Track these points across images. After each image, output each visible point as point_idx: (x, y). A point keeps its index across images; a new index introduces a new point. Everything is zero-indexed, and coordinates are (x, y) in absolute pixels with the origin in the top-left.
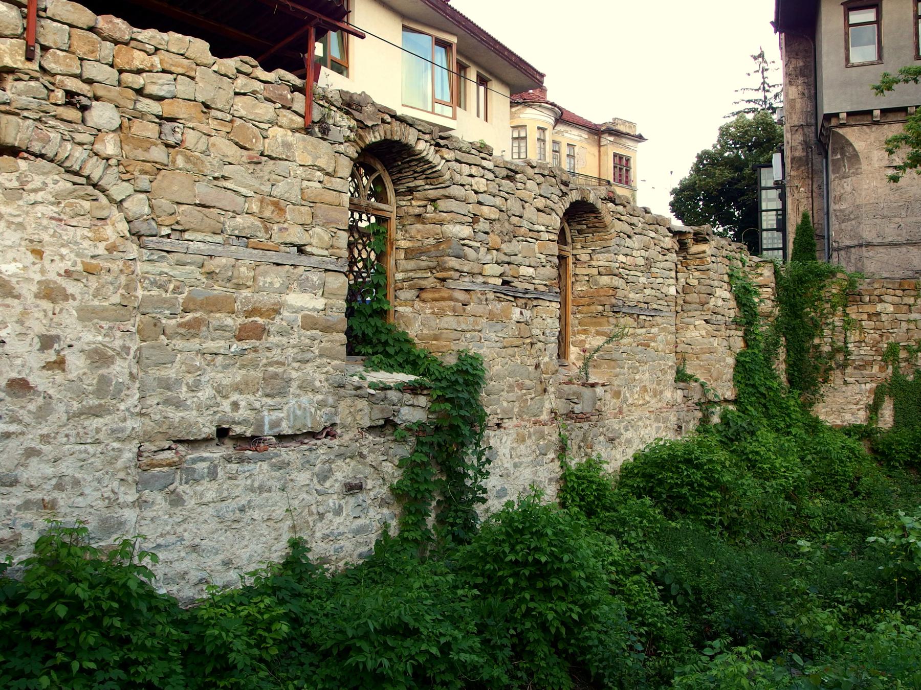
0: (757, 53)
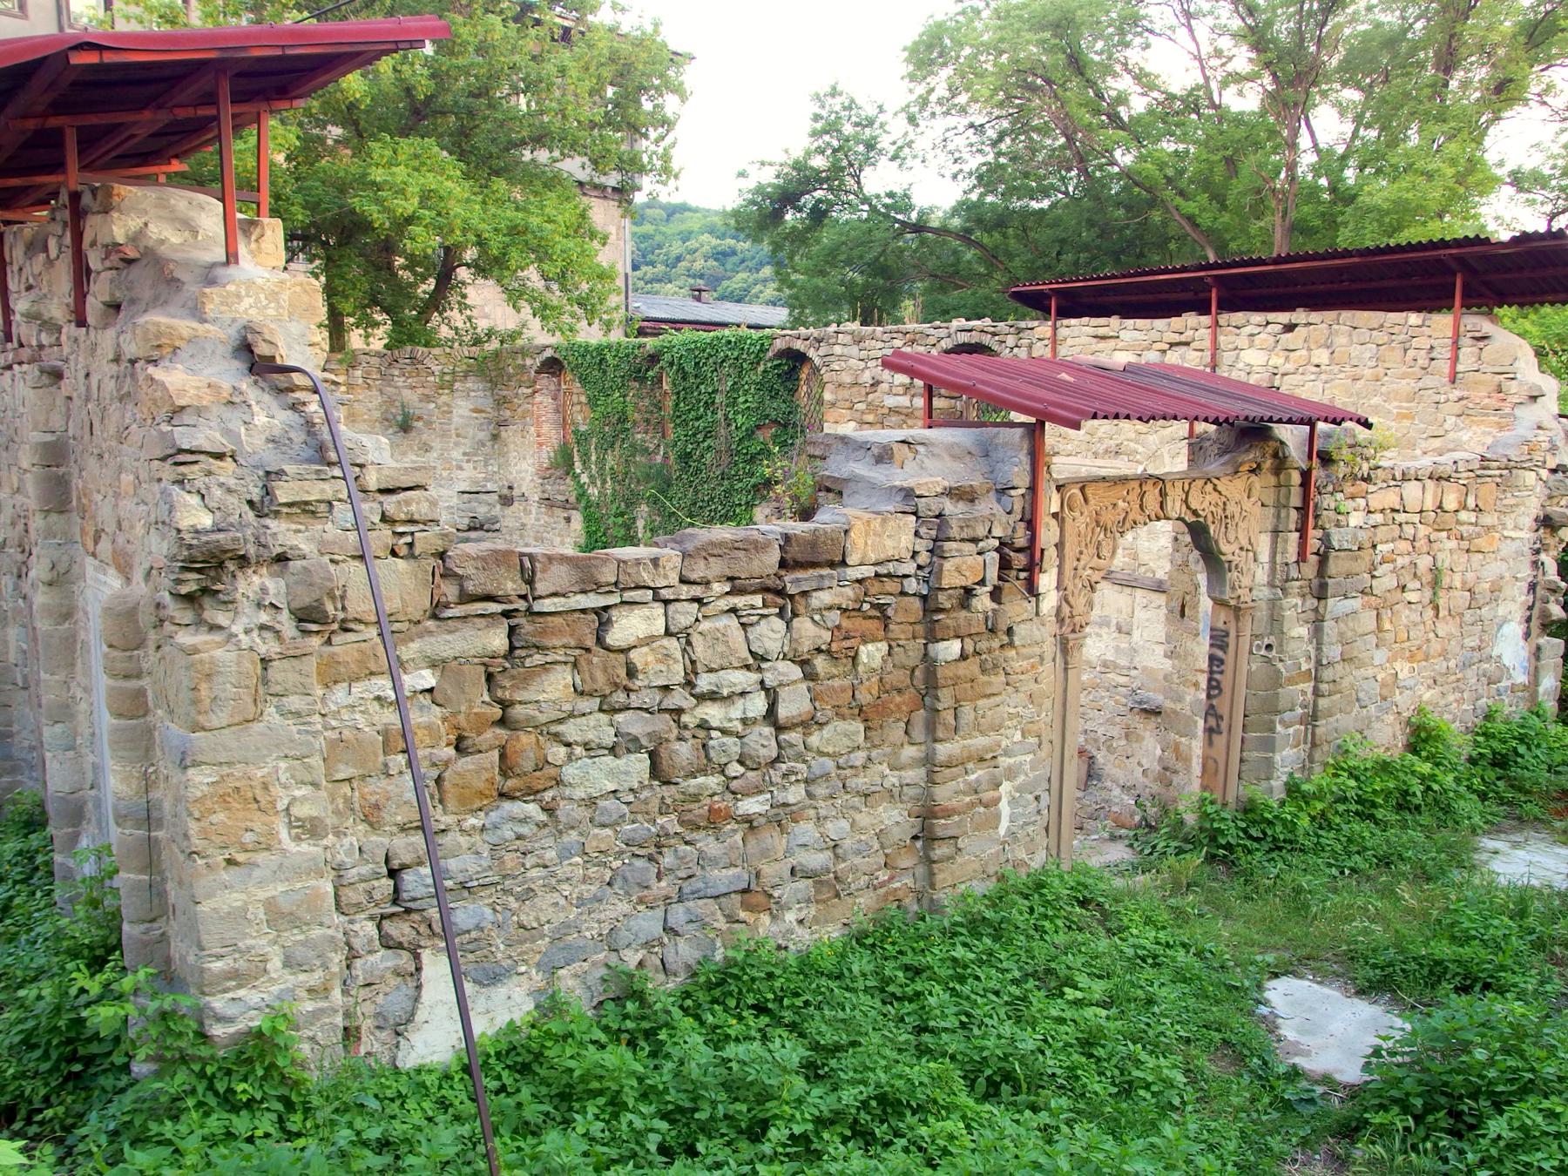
0: (839, 88)
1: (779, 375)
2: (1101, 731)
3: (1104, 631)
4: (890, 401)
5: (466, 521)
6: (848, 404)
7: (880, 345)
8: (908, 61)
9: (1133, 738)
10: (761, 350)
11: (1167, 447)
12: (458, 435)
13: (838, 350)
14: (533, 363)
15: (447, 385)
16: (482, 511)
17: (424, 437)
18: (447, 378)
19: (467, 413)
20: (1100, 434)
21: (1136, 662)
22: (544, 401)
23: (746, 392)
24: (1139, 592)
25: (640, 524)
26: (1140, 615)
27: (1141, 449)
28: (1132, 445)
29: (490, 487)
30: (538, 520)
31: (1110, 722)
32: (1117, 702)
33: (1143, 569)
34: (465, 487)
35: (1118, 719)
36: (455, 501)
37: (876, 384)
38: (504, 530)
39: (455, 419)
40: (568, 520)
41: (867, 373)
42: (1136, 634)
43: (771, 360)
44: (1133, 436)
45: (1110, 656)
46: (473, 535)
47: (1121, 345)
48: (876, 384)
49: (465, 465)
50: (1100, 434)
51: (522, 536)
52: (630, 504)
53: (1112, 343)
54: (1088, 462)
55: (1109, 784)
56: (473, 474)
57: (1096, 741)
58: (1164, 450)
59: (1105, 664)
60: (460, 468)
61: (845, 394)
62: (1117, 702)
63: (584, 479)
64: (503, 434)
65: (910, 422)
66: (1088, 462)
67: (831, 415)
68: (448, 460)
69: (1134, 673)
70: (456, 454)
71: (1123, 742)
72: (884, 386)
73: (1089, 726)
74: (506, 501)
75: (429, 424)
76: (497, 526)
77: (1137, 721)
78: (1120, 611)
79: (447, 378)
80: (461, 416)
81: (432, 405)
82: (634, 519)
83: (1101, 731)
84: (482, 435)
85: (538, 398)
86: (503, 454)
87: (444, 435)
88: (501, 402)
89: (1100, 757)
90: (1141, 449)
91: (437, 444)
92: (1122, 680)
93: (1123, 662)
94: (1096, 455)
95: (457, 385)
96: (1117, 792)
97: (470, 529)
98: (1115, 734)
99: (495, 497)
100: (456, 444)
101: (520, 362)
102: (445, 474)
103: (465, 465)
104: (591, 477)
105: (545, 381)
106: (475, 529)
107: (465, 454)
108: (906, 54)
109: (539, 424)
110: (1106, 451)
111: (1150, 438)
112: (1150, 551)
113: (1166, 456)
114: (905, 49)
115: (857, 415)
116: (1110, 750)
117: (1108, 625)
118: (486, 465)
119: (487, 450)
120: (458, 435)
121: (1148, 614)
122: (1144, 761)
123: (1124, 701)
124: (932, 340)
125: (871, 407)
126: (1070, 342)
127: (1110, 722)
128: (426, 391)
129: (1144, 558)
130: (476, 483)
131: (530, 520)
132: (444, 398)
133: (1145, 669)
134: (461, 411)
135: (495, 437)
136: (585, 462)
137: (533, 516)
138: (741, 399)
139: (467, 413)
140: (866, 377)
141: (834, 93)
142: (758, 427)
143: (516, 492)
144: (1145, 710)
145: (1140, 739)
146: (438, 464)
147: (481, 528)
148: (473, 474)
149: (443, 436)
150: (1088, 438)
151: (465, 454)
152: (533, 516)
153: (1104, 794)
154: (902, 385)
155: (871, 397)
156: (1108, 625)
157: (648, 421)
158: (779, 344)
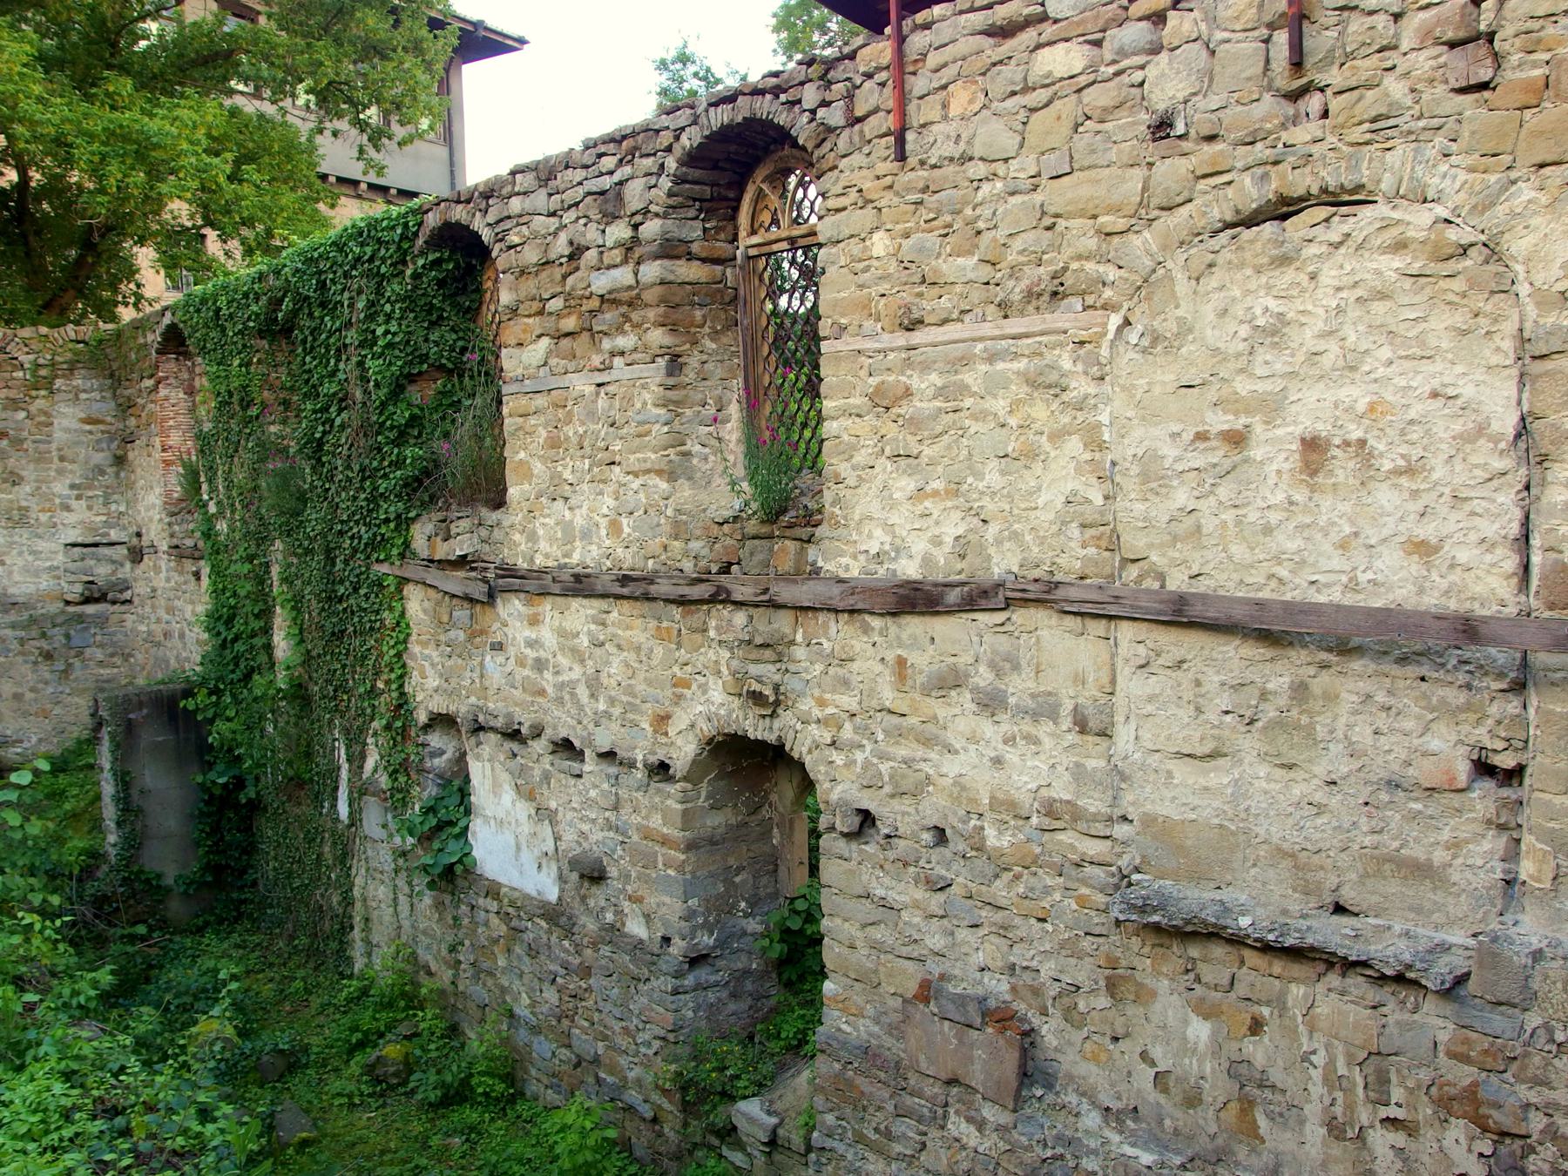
1: (441, 283)
2: (1048, 969)
3: (1044, 729)
4: (601, 283)
5: (79, 588)
6: (536, 306)
7: (579, 174)
8: (776, 30)
9: (1126, 990)
10: (403, 237)
11: (1181, 256)
12: (62, 459)
13: (516, 205)
14: (154, 338)
15: (42, 383)
16: (102, 572)
17: (11, 462)
18: (43, 372)
19: (75, 425)
20: (1012, 257)
21: (1129, 801)
22: (173, 395)
23: (389, 317)
24: (1126, 631)
25: (275, 571)
26: (1132, 686)
27: (1112, 273)
28: (1090, 266)
29: (114, 535)
30: (168, 580)
31: (1068, 948)
32: (1082, 902)
33: (1133, 572)
34: (74, 535)
35: (1087, 944)
36: (59, 560)
37: (576, 252)
38: (136, 600)
39: (58, 435)
40: (197, 575)
41: (563, 238)
42: (1124, 735)
43: (422, 253)
44: (1091, 243)
45: (1061, 791)
46: (90, 609)
47: (1049, 30)
48: (576, 252)
49: (74, 504)
50: (1012, 257)
51: (153, 607)
52: (262, 540)
53: (1028, 37)
54: (987, 329)
55: (1072, 1098)
56: (87, 516)
57: (1036, 992)
58: (1175, 263)
59: (1050, 810)
60: (67, 508)
61: (529, 286)
62: (1082, 902)
63: (212, 509)
64: (131, 455)
65: (635, 316)
66: (987, 329)
67: (510, 334)
68: (48, 498)
69: (1121, 831)
70: (60, 488)
71: (1103, 1001)
72: (591, 255)
73: (1018, 956)
74: (137, 555)
75: (17, 443)
76: (127, 595)
77: (1138, 956)
78: (1079, 680)
79: (43, 372)
80: (67, 430)
81: (23, 414)
82: (267, 565)
83: (1048, 969)
84: (100, 458)
85: (163, 392)
86: (131, 486)
87: (41, 459)
88: (126, 407)
89: (1050, 1031)
90: (1112, 273)
91: (29, 472)
92: (1094, 848)
93: (1094, 804)
94: (1005, 309)
95: (58, 383)
96: (1092, 1119)
97: (87, 600)
98: (1081, 978)
99: (123, 551)
100: (60, 472)
101: (142, 341)
102: (44, 517)
103: (74, 504)
104: (219, 503)
105: (169, 366)
106: (97, 601)
107: (72, 487)
108: (774, 21)
109: (164, 433)
110: (1031, 295)
111: (1135, 241)
112: (1148, 525)
113: (1180, 276)
114: (775, 15)
115: (549, 323)
116: (1071, 1016)
117: (1054, 716)
118: (106, 504)
119: (108, 479)
120: (62, 459)
121: (1153, 684)
122: (1157, 1052)
123: (1101, 899)
124: (666, 138)
125: (573, 302)
126: (933, 60)
127: (1068, 948)
128: (13, 394)
129: (1134, 542)
130: (92, 529)
131: (160, 582)
132: (40, 403)
133: (1149, 821)
134: (65, 423)
135: (120, 461)
136: (213, 490)
137: (163, 575)
138: (380, 331)
139: (75, 425)
140: (561, 247)
141: (684, 59)
142: (412, 379)
143: (145, 542)
144: (1157, 928)
145: (1144, 996)
146: (33, 504)
147: (102, 598)
148: (87, 516)
149: (38, 461)
150: (985, 272)
151: (72, 487)
152: (163, 575)
153: (1061, 1123)
154: (619, 244)
155: (570, 281)
156: (1054, 716)
157: (286, 404)
158: (432, 220)
